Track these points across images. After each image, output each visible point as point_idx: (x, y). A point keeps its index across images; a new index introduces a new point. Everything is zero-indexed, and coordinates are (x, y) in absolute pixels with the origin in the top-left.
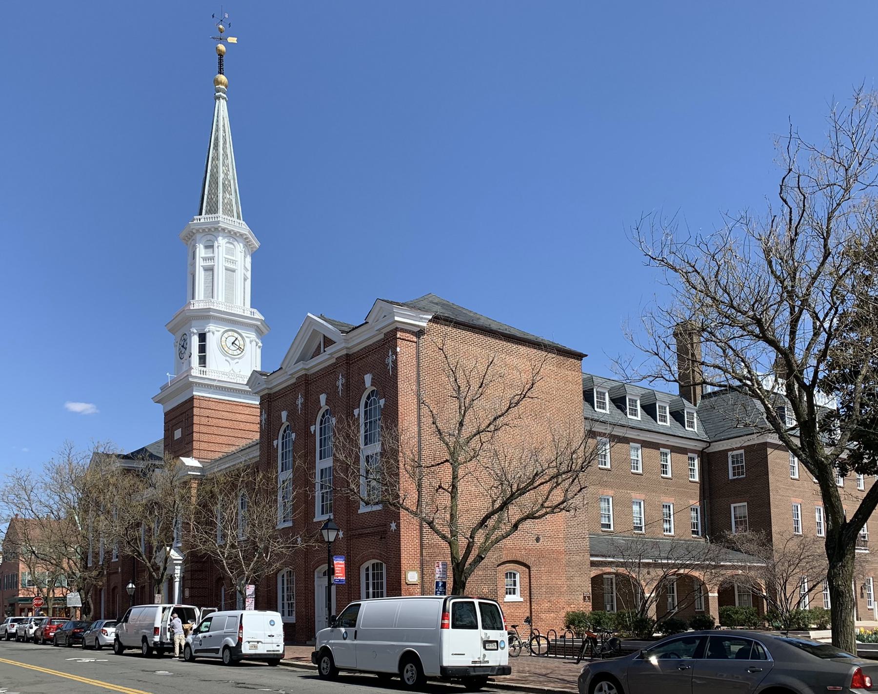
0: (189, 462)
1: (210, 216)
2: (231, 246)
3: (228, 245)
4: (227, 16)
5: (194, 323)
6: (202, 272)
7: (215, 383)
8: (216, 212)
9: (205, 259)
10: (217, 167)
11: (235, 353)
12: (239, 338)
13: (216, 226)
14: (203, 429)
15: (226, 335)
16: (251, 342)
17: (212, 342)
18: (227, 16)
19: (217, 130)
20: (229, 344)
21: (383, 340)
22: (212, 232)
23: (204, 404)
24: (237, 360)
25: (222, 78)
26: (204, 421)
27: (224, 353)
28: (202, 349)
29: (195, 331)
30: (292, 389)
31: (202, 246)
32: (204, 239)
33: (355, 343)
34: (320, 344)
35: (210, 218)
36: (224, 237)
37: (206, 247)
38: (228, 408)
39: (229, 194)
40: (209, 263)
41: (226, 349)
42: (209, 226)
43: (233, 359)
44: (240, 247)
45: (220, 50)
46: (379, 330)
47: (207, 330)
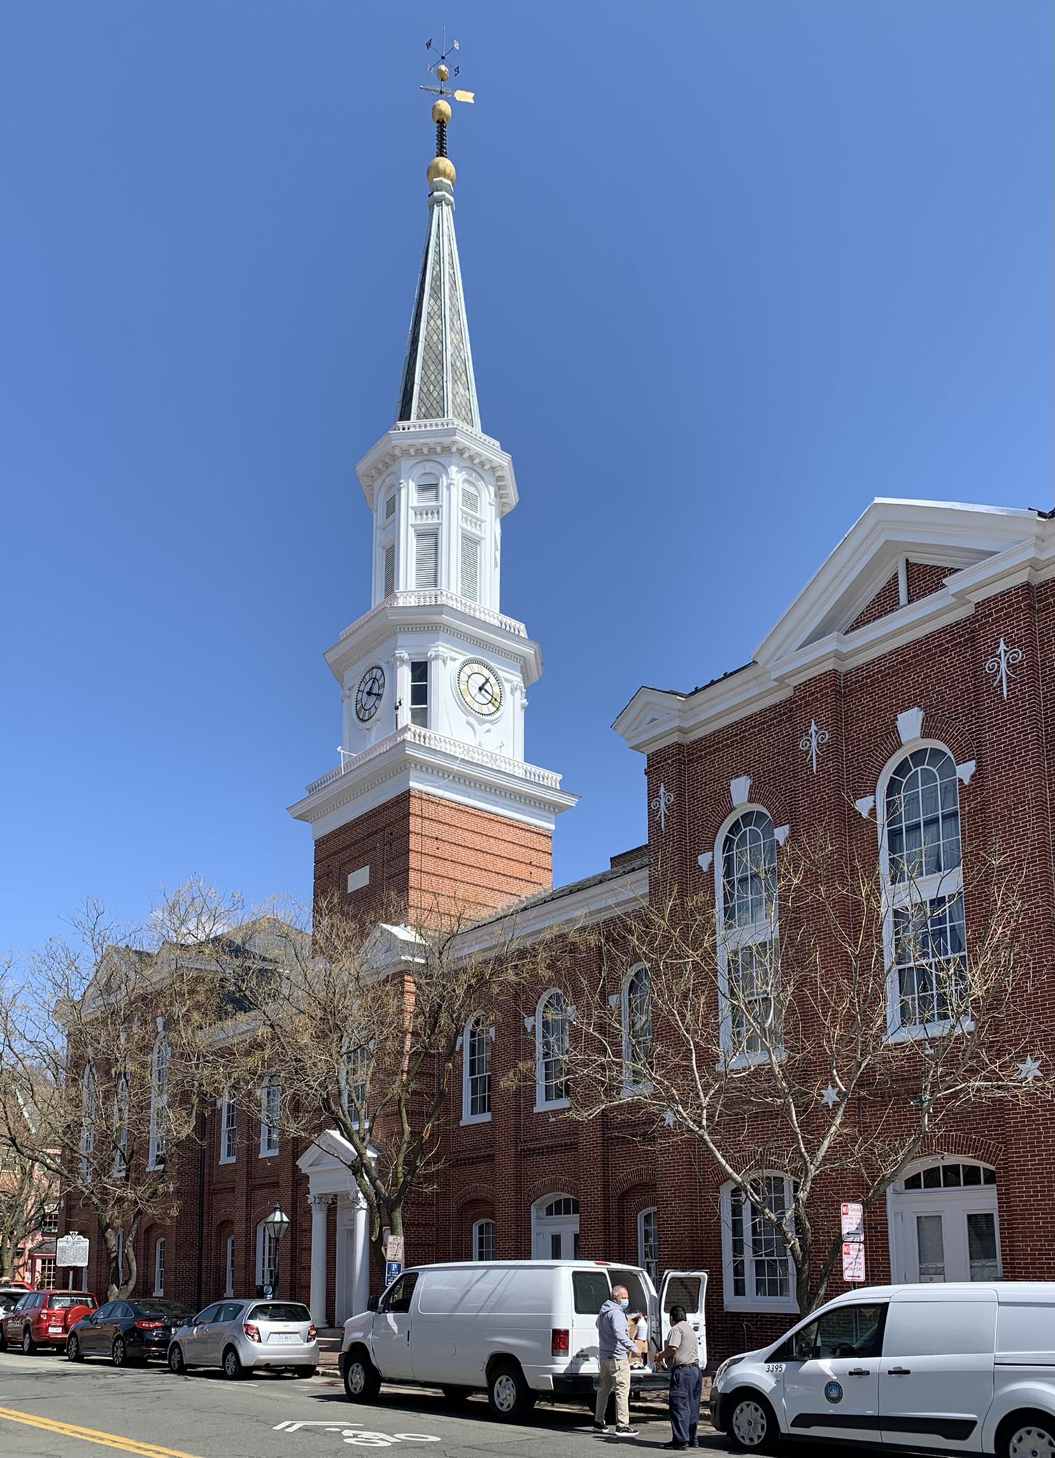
0: (403, 933)
1: (428, 422)
2: (472, 490)
3: (467, 487)
4: (457, 46)
5: (402, 639)
6: (413, 541)
7: (456, 766)
8: (442, 413)
9: (419, 512)
10: (440, 332)
11: (485, 710)
12: (492, 680)
13: (447, 441)
14: (429, 864)
15: (467, 670)
16: (513, 691)
17: (442, 679)
18: (457, 46)
19: (438, 262)
20: (474, 691)
21: (972, 619)
22: (439, 453)
23: (430, 810)
24: (488, 726)
25: (445, 163)
26: (430, 847)
27: (466, 708)
28: (420, 695)
29: (406, 656)
30: (786, 716)
31: (412, 485)
32: (419, 470)
33: (703, 717)
34: (896, 576)
35: (432, 424)
36: (461, 469)
37: (422, 488)
38: (475, 824)
39: (462, 391)
40: (430, 520)
41: (468, 699)
42: (431, 441)
43: (482, 723)
44: (487, 495)
45: (441, 113)
46: (780, 679)
47: (432, 653)
